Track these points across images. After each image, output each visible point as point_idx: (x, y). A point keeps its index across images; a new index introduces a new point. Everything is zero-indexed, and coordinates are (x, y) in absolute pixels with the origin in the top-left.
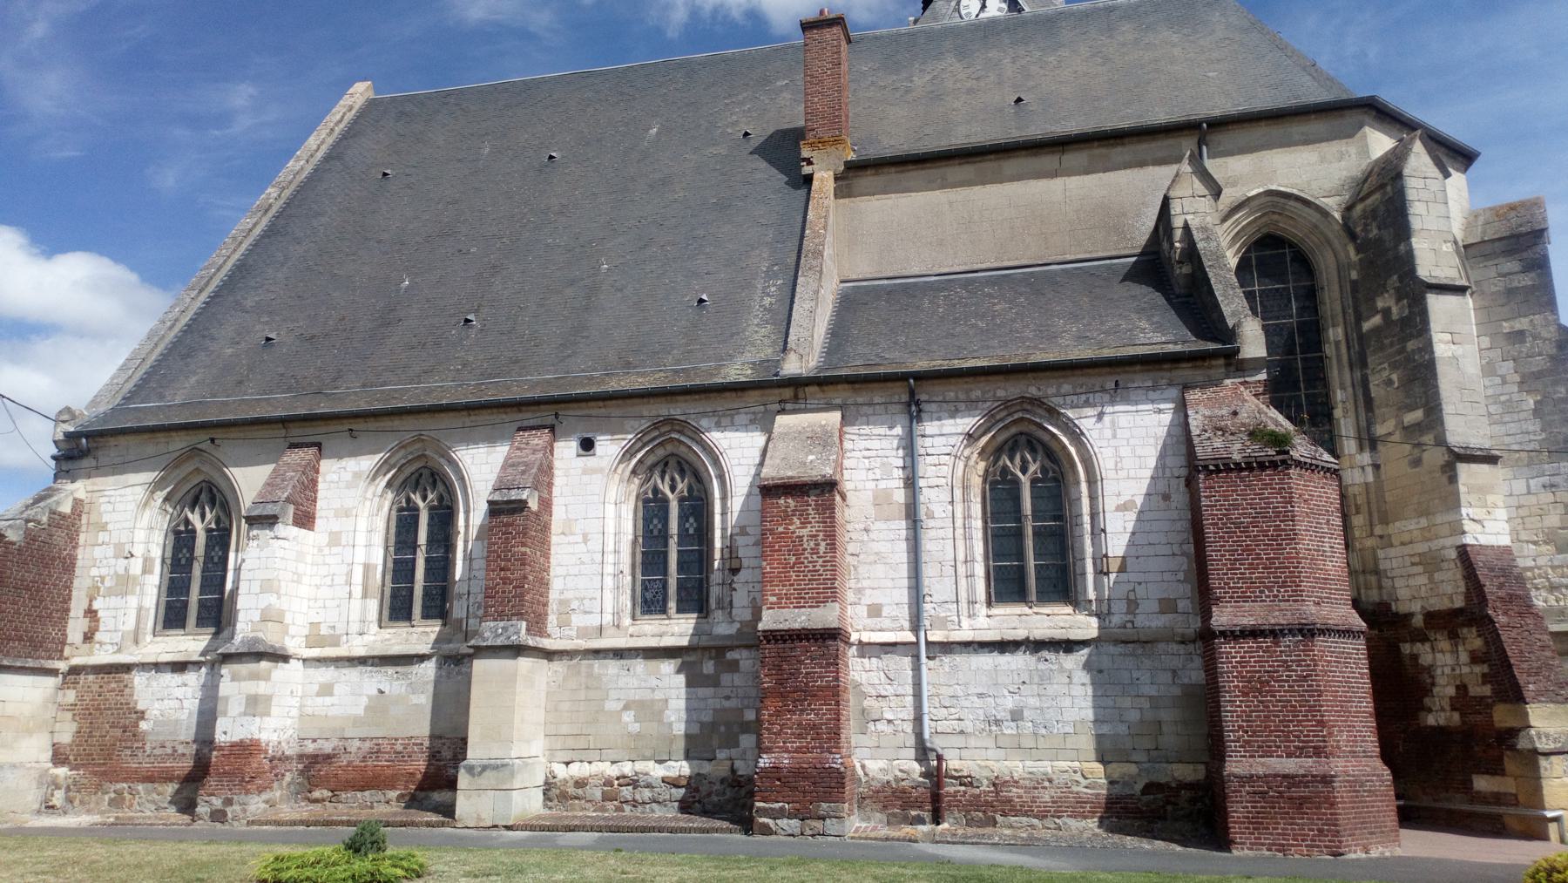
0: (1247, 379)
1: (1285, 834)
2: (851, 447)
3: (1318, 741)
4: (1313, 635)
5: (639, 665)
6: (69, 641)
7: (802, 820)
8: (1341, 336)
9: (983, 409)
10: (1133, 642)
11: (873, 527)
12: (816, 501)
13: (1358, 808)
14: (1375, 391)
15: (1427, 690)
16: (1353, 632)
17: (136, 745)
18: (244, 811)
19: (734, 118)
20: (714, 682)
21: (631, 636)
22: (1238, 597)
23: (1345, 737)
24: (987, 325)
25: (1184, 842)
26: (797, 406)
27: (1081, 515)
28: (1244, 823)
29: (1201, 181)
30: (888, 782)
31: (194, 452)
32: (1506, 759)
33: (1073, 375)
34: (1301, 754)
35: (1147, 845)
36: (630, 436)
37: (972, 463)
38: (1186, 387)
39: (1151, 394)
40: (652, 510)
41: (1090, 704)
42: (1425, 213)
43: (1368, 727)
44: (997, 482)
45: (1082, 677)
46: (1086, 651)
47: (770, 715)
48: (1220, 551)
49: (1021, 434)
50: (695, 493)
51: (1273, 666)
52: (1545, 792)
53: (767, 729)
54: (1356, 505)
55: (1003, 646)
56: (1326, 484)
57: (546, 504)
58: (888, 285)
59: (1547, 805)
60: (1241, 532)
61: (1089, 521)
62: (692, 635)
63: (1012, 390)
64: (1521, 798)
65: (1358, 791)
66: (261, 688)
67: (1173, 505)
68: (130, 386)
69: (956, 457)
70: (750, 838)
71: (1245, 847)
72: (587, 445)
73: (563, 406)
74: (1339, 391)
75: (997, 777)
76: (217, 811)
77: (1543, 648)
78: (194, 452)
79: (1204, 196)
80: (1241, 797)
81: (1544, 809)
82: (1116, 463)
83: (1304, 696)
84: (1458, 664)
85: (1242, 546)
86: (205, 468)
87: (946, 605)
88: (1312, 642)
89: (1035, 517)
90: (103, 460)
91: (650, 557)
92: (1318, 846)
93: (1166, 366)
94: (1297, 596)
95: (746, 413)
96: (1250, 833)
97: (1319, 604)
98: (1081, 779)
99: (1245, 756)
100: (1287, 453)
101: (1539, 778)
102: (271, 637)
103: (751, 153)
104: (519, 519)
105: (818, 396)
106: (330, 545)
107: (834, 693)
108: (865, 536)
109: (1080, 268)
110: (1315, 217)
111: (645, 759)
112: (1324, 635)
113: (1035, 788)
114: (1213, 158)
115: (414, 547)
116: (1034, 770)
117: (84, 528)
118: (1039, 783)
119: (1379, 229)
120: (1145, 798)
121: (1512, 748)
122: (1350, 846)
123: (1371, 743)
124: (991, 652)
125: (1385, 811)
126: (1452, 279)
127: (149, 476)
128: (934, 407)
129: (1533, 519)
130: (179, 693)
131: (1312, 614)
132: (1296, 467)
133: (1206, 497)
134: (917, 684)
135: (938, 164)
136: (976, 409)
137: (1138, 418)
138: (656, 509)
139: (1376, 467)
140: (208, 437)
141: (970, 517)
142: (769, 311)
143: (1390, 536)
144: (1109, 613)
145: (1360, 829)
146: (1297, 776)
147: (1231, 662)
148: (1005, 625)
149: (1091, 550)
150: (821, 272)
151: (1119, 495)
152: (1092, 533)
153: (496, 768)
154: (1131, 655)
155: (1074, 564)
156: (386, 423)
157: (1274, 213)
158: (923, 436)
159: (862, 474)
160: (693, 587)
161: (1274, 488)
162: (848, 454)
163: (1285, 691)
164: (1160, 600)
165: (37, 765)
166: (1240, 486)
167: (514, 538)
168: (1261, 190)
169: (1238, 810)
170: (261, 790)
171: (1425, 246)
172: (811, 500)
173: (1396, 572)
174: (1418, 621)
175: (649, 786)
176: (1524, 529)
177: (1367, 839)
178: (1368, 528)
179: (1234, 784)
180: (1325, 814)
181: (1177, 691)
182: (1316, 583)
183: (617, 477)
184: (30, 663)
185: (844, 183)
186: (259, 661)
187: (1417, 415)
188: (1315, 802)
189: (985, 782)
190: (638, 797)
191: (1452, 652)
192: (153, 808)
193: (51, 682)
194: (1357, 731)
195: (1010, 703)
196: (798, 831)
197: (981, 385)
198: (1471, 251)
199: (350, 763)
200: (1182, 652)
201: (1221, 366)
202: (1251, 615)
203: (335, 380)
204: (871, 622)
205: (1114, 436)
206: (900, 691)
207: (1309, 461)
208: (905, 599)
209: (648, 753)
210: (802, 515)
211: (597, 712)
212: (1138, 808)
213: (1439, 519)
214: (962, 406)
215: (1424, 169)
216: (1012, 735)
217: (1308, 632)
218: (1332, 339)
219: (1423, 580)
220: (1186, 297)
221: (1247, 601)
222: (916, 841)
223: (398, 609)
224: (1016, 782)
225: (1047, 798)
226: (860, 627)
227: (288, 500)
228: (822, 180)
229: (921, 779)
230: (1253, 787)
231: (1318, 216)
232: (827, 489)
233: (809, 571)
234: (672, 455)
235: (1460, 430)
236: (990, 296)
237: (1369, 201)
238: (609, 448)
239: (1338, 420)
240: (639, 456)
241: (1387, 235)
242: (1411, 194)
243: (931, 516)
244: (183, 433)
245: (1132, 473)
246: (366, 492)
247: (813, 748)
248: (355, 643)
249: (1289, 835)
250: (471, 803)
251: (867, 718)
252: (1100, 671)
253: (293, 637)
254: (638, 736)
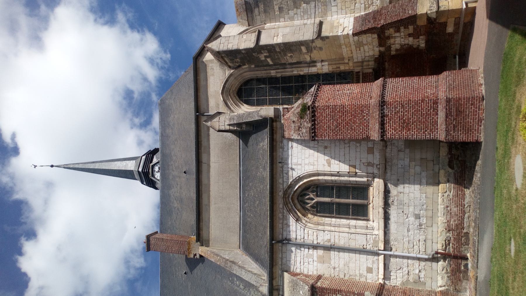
0: (282, 114)
2: (299, 269)
3: (431, 102)
4: (384, 101)
8: (274, 71)
9: (287, 214)
11: (333, 266)
13: (461, 87)
14: (295, 61)
15: (410, 47)
16: (384, 84)
19: (180, 275)
22: (367, 129)
23: (429, 91)
24: (258, 200)
25: (477, 159)
26: (281, 290)
29: (214, 119)
32: (440, 22)
34: (436, 109)
37: (308, 220)
38: (283, 137)
39: (285, 149)
41: (413, 186)
42: (232, 44)
43: (425, 80)
45: (401, 188)
46: (389, 185)
48: (347, 134)
51: (397, 118)
52: (455, 8)
54: (336, 68)
55: (387, 218)
59: (460, 7)
60: (340, 126)
61: (334, 177)
64: (457, 16)
67: (329, 145)
69: (305, 227)
71: (479, 136)
74: (294, 73)
75: (446, 229)
77: (394, 7)
79: (219, 118)
80: (456, 135)
81: (462, 9)
83: (410, 107)
84: (400, 36)
87: (368, 239)
89: (332, 197)
93: (275, 144)
94: (368, 106)
97: (371, 97)
98: (447, 194)
100: (309, 106)
101: (449, 10)
103: (192, 274)
108: (337, 269)
109: (242, 160)
110: (232, 78)
112: (384, 96)
113: (451, 213)
114: (209, 111)
116: (442, 213)
118: (449, 212)
119: (237, 58)
120: (456, 168)
121: (435, 19)
122: (479, 92)
123: (432, 79)
125: (463, 75)
126: (255, 36)
128: (285, 233)
129: (346, 5)
131: (375, 101)
132: (315, 103)
133: (325, 138)
134: (403, 257)
135: (201, 207)
136: (287, 216)
137: (294, 155)
139: (322, 61)
141: (330, 224)
142: (245, 287)
143: (348, 57)
144: (373, 174)
145: (471, 87)
146: (446, 112)
147: (395, 134)
148: (377, 216)
149: (346, 177)
151: (324, 165)
152: (339, 176)
154: (391, 167)
157: (229, 92)
158: (296, 239)
159: (311, 267)
161: (323, 112)
168: (221, 96)
169: (462, 137)
171: (243, 44)
173: (363, 55)
174: (382, 49)
176: (350, 7)
177: (476, 84)
179: (450, 138)
180: (464, 102)
182: (362, 98)
185: (204, 242)
187: (304, 49)
189: (448, 234)
191: (395, 38)
195: (412, 219)
198: (251, 23)
202: (375, 125)
204: (375, 273)
205: (301, 165)
206: (406, 264)
207: (313, 97)
213: (342, 42)
214: (285, 222)
215: (217, 44)
216: (426, 219)
217: (382, 103)
218: (275, 74)
219: (366, 47)
220: (254, 127)
221: (369, 125)
224: (448, 221)
225: (456, 209)
226: (377, 278)
228: (202, 252)
229: (447, 261)
230: (451, 130)
231: (232, 77)
232: (314, 289)
235: (309, 35)
236: (248, 195)
237: (227, 61)
239: (304, 73)
241: (239, 56)
242: (225, 48)
243: (329, 241)
245: (316, 159)
249: (474, 117)
251: (418, 281)
252: (398, 180)
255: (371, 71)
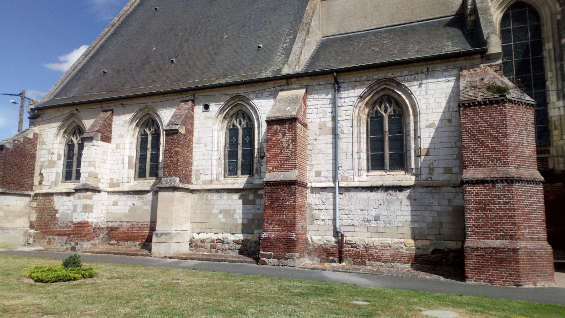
0: (492, 64)
1: (493, 275)
4: (512, 183)
5: (225, 196)
6: (34, 185)
7: (278, 259)
9: (367, 85)
10: (430, 187)
11: (318, 138)
12: (289, 126)
13: (531, 264)
16: (536, 182)
17: (55, 222)
18: (82, 247)
20: (253, 203)
21: (223, 184)
22: (476, 165)
26: (288, 87)
27: (409, 131)
28: (473, 269)
30: (321, 245)
31: (72, 115)
33: (409, 67)
34: (503, 238)
35: (428, 276)
36: (223, 103)
37: (362, 109)
38: (461, 69)
39: (445, 74)
40: (232, 133)
44: (374, 117)
45: (407, 202)
46: (409, 191)
47: (267, 216)
48: (469, 144)
49: (385, 95)
50: (249, 126)
51: (492, 197)
53: (266, 222)
55: (372, 189)
56: (527, 111)
57: (190, 132)
58: (342, 37)
60: (479, 134)
61: (413, 133)
62: (245, 184)
63: (380, 75)
65: (533, 256)
66: (88, 202)
67: (453, 124)
68: (57, 91)
69: (354, 106)
70: (258, 266)
72: (206, 107)
73: (197, 91)
75: (367, 245)
76: (73, 247)
78: (72, 115)
80: (472, 257)
82: (427, 107)
83: (506, 211)
85: (480, 141)
86: (76, 121)
87: (348, 171)
88: (512, 186)
89: (390, 132)
90: (44, 119)
91: (231, 153)
92: (509, 281)
95: (268, 92)
96: (475, 274)
97: (518, 168)
99: (475, 239)
100: (505, 96)
102: (92, 183)
104: (176, 137)
105: (297, 83)
106: (116, 149)
107: (293, 208)
108: (315, 142)
111: (227, 233)
115: (146, 149)
116: (383, 242)
117: (38, 144)
120: (433, 256)
123: (542, 234)
124: (366, 191)
125: (547, 266)
127: (58, 124)
128: (345, 85)
130: (68, 203)
131: (512, 173)
132: (509, 102)
133: (463, 118)
134: (334, 205)
136: (364, 85)
137: (438, 85)
138: (234, 133)
140: (74, 109)
141: (360, 133)
144: (420, 174)
145: (532, 274)
146: (500, 248)
148: (373, 180)
150: (308, 32)
152: (415, 138)
153: (166, 234)
154: (429, 192)
155: (406, 153)
156: (135, 101)
158: (340, 98)
159: (314, 116)
160: (248, 165)
161: (497, 113)
162: (309, 107)
163: (497, 209)
164: (444, 168)
165: (23, 229)
166: (480, 113)
167: (174, 145)
169: (470, 263)
170: (88, 240)
172: (287, 126)
175: (228, 243)
177: (535, 279)
178: (560, 136)
180: (513, 266)
181: (450, 209)
183: (218, 120)
184: (19, 192)
186: (86, 192)
188: (509, 261)
189: (362, 246)
190: (224, 247)
192: (60, 245)
193: (27, 199)
194: (535, 228)
195: (374, 213)
196: (276, 264)
197: (366, 74)
199: (123, 231)
200: (453, 191)
201: (478, 58)
202: (482, 174)
203: (123, 86)
205: (427, 94)
206: (328, 207)
207: (517, 100)
208: (331, 169)
209: (228, 231)
210: (283, 133)
211: (209, 214)
212: (429, 260)
214: (358, 84)
217: (510, 181)
221: (481, 167)
222: (325, 270)
223: (141, 174)
225: (388, 254)
226: (312, 181)
227: (98, 131)
230: (478, 253)
233: (285, 156)
234: (240, 110)
236: (384, 37)
238: (215, 108)
239: (548, 86)
240: (226, 111)
243: (343, 133)
244: (68, 107)
245: (434, 111)
246: (128, 128)
247: (284, 230)
248: (125, 186)
249: (495, 275)
250: (157, 248)
251: (314, 218)
252: (415, 200)
253: (103, 183)
254: (224, 224)
255: (551, 166)
